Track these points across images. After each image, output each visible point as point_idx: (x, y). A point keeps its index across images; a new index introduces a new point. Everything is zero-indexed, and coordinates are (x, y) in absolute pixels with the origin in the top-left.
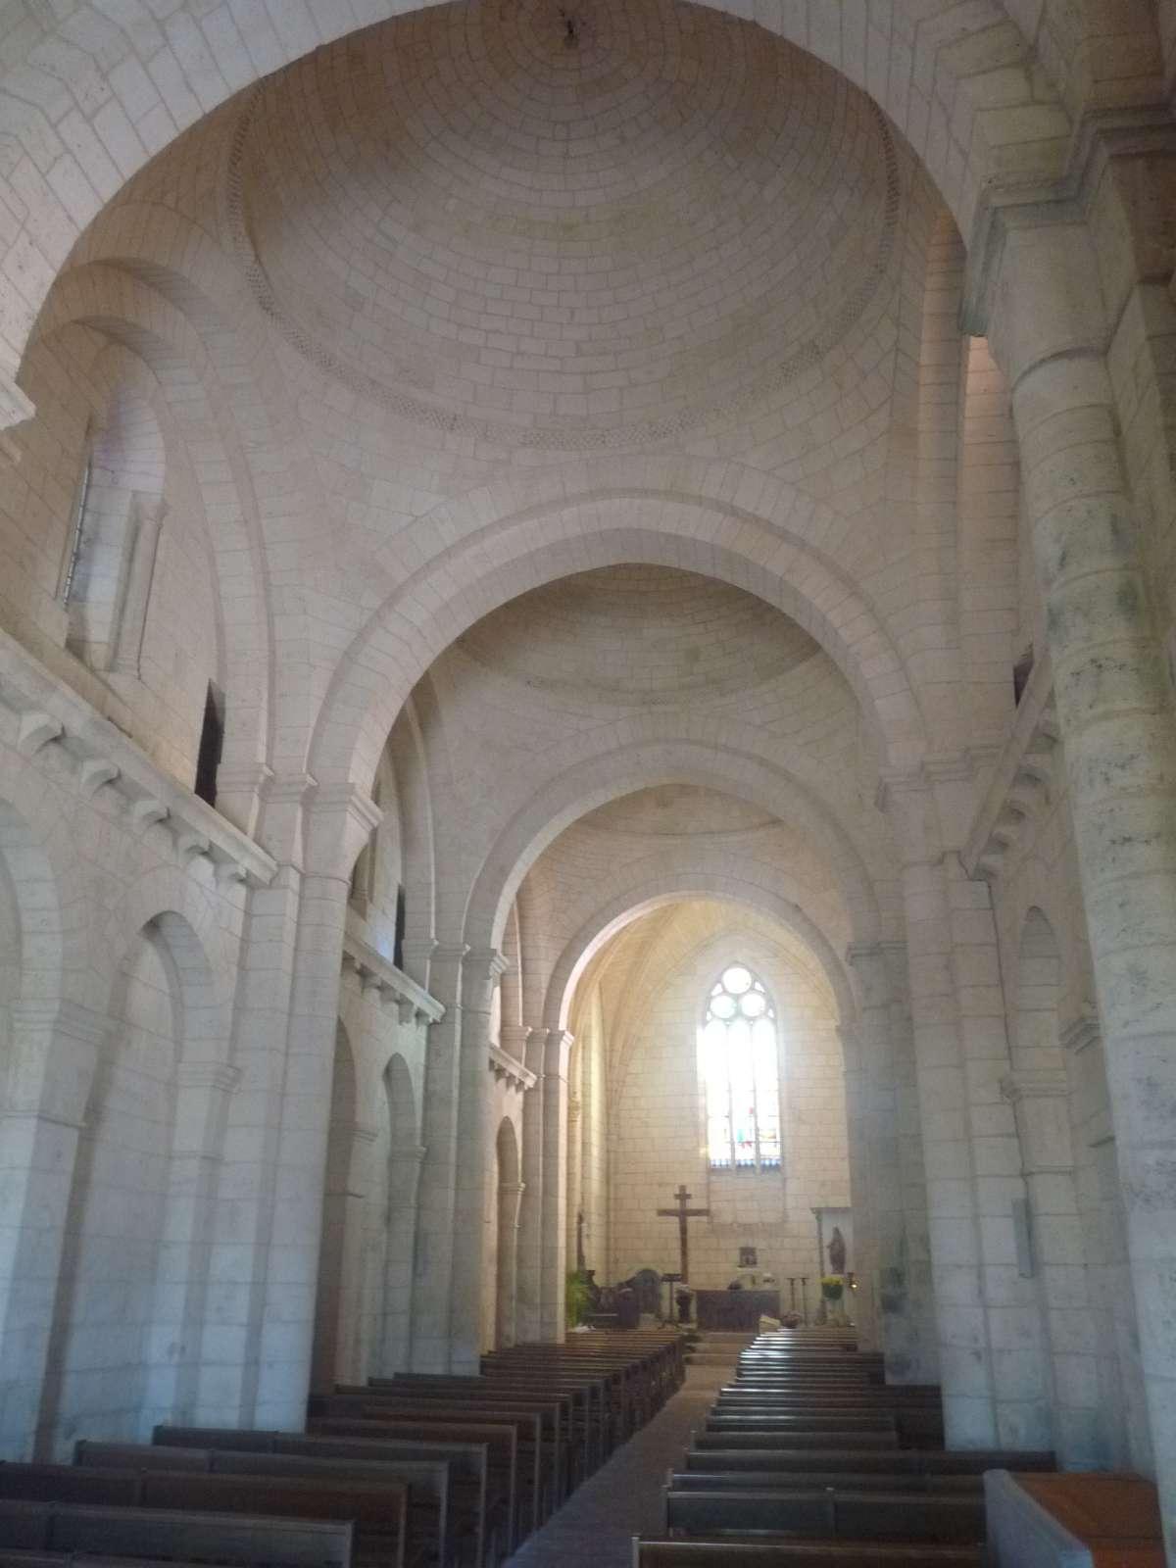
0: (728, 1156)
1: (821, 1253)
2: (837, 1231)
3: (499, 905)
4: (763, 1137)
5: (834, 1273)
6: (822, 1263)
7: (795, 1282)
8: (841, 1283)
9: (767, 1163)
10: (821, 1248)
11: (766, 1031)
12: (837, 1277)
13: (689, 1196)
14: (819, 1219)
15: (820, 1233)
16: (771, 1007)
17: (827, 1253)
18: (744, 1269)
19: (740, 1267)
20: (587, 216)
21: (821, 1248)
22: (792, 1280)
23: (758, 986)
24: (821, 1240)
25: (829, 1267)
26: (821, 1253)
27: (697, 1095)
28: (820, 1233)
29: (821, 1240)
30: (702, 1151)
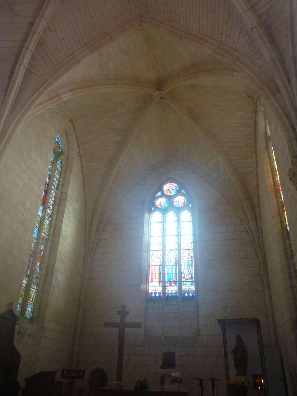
0: (158, 282)
1: (226, 357)
2: (239, 338)
3: (64, 221)
4: (185, 278)
5: (237, 375)
6: (227, 365)
7: (204, 382)
8: (246, 384)
9: (186, 295)
10: (226, 353)
11: (186, 215)
12: (242, 379)
13: (128, 313)
14: (224, 330)
15: (225, 342)
16: (190, 202)
17: (231, 356)
18: (164, 370)
19: (161, 368)
20: (187, 19)
21: (226, 353)
22: (201, 381)
23: (183, 191)
24: (225, 346)
25: (233, 370)
26: (226, 357)
27: (69, 72)
28: (225, 342)
29: (225, 346)
30: (143, 287)
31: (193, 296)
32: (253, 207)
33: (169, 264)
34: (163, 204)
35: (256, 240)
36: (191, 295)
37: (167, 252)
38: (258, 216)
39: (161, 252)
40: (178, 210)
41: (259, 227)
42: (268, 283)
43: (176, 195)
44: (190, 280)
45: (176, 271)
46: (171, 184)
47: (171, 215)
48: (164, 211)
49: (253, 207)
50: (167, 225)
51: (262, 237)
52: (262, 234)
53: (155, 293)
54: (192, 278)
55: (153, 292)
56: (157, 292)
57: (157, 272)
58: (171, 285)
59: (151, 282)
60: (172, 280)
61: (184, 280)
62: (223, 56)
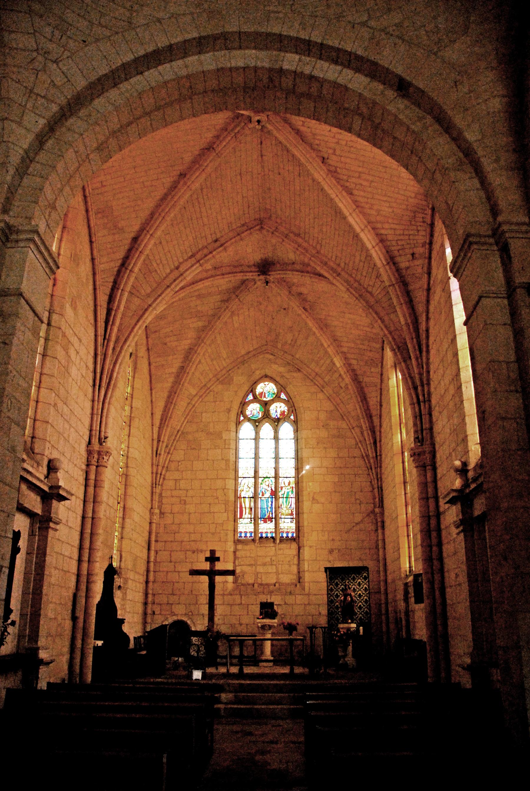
4: (283, 514)
31: (293, 536)
32: (373, 430)
33: (263, 495)
34: (255, 412)
35: (373, 469)
36: (290, 535)
37: (260, 480)
38: (115, 308)
39: (253, 480)
40: (277, 422)
41: (107, 337)
42: (383, 522)
43: (273, 401)
44: (290, 517)
45: (272, 505)
46: (266, 383)
47: (267, 429)
48: (257, 423)
49: (373, 430)
50: (262, 443)
51: (381, 467)
52: (381, 464)
53: (246, 533)
54: (292, 514)
55: (264, 531)
56: (248, 530)
57: (247, 506)
58: (265, 522)
59: (241, 517)
60: (266, 517)
61: (282, 517)
62: (337, 196)
